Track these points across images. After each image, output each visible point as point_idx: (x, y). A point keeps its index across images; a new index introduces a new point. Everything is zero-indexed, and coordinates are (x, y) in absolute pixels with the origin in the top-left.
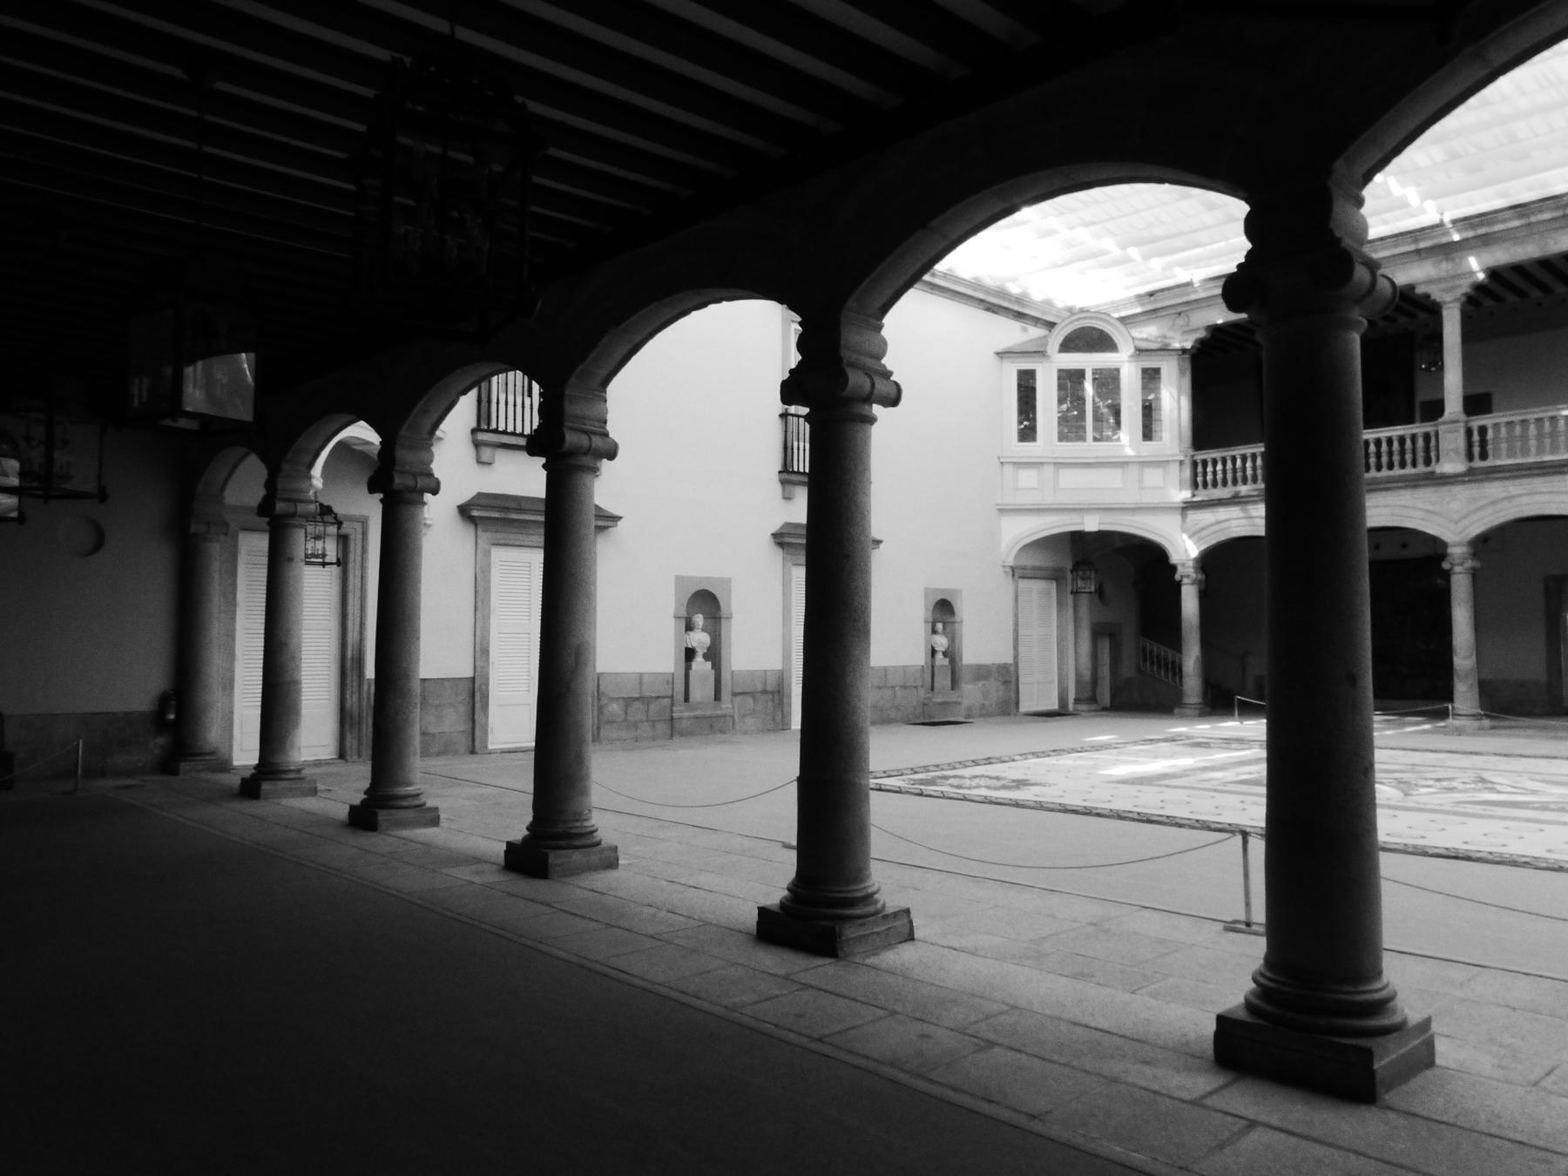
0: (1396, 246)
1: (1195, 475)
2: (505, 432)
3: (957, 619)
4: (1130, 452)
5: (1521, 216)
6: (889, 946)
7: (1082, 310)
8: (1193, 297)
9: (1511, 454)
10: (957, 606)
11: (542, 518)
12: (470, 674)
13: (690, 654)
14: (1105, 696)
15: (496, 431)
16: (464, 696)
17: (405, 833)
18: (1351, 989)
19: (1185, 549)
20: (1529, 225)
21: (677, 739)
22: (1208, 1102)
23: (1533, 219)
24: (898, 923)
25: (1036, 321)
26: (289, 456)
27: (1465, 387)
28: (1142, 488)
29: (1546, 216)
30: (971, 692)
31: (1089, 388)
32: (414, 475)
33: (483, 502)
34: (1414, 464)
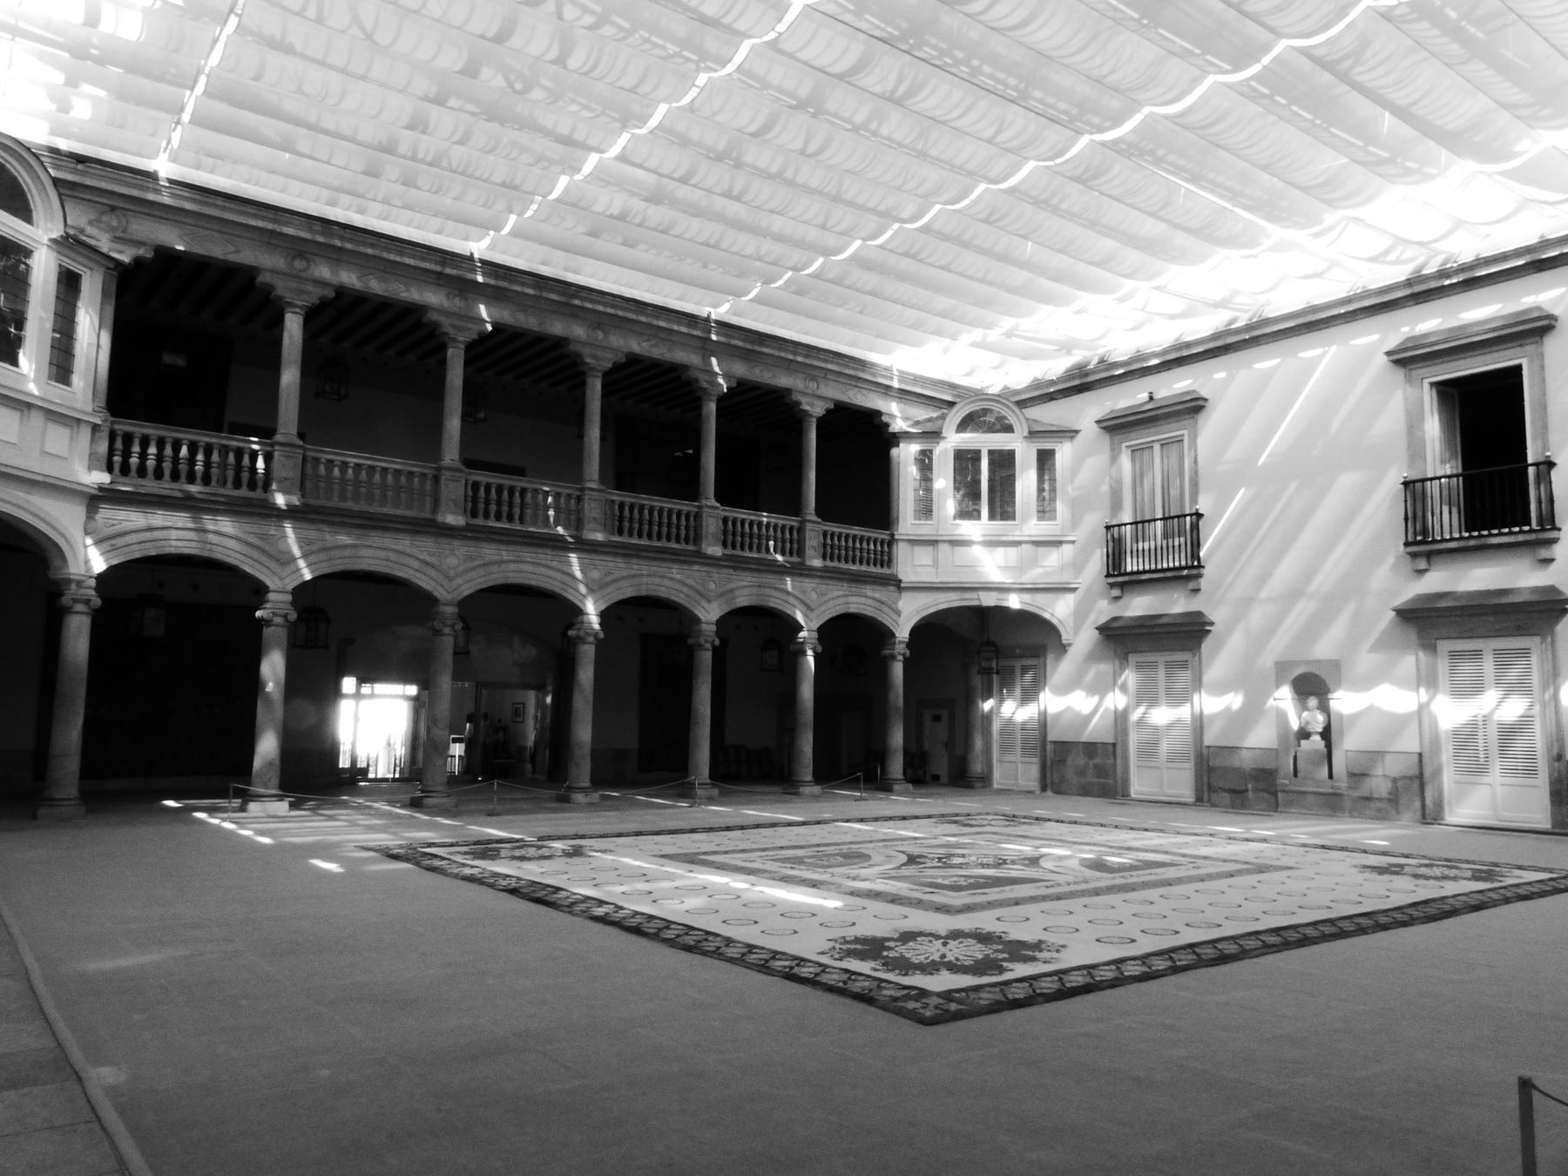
0: (424, 259)
5: (535, 287)
8: (151, 197)
9: (396, 504)
20: (540, 298)
23: (545, 294)
29: (554, 297)
34: (742, 548)
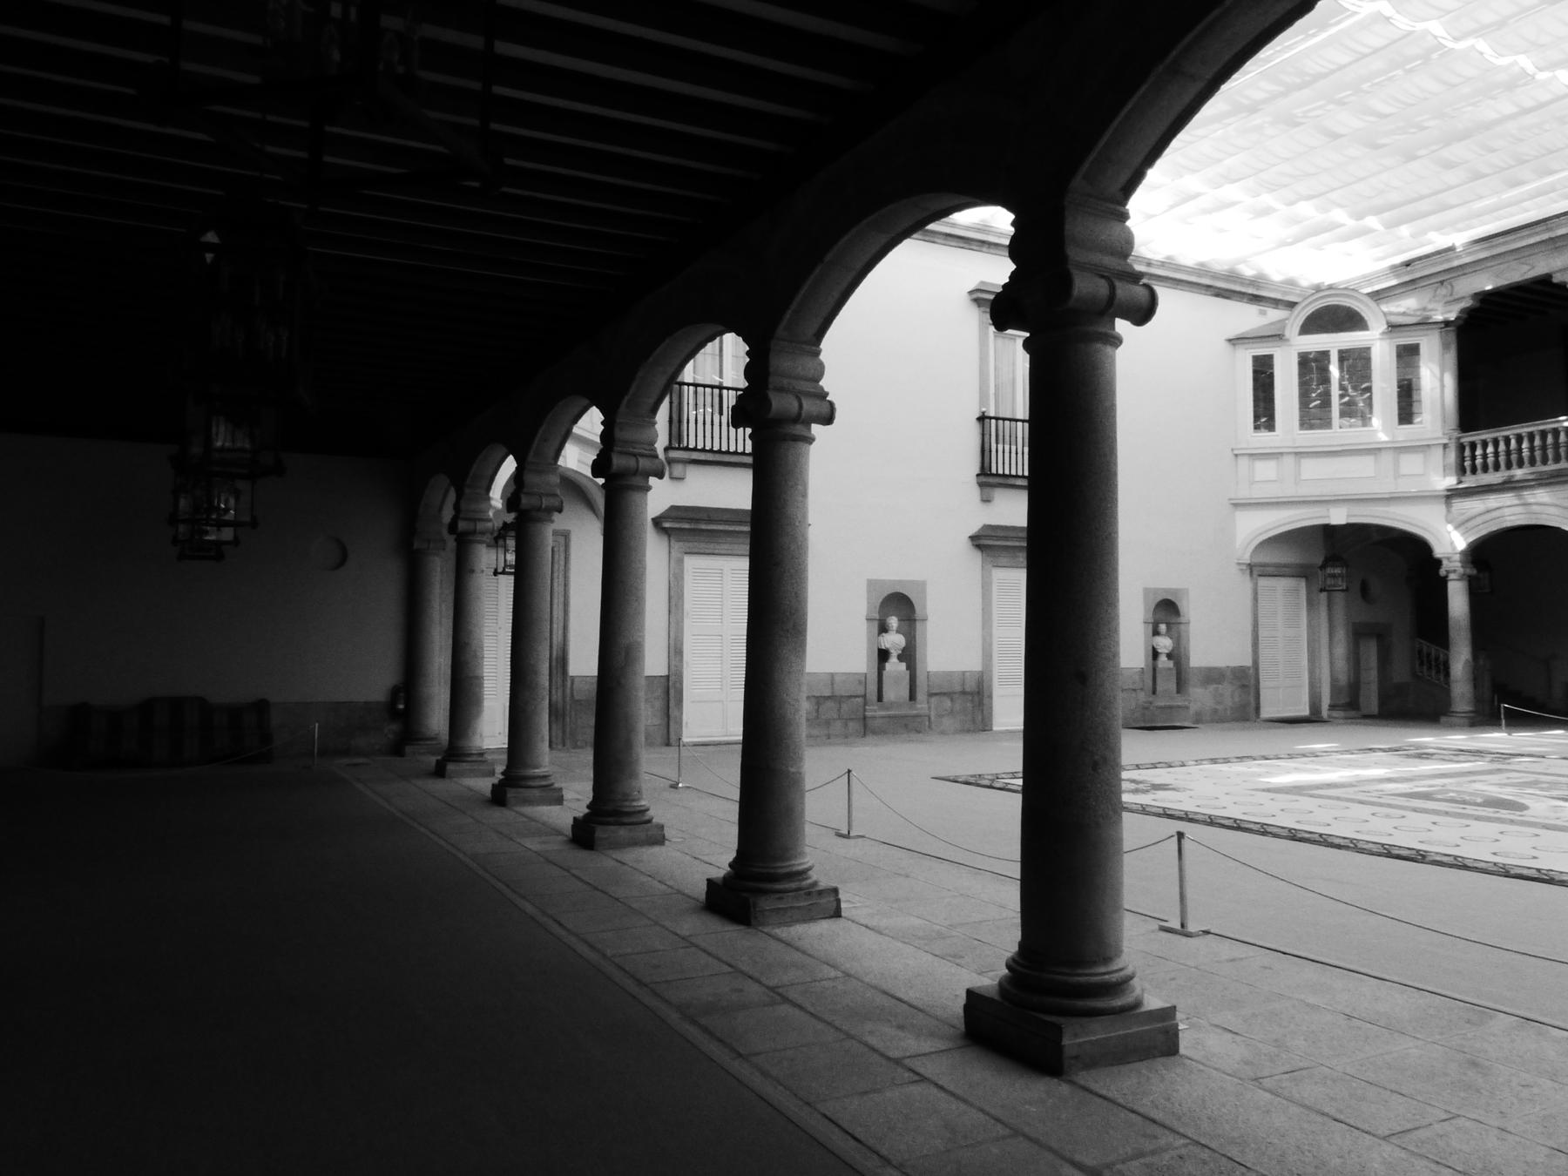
1: (1462, 459)
2: (695, 449)
3: (1182, 619)
4: (1383, 437)
6: (811, 919)
7: (1330, 287)
8: (1456, 263)
10: (1183, 606)
11: (747, 528)
12: (664, 672)
13: (883, 655)
14: (1371, 701)
15: (687, 449)
16: (659, 692)
17: (528, 810)
18: (1103, 970)
19: (1451, 540)
21: (870, 738)
22: (907, 1062)
24: (823, 901)
25: (1276, 303)
26: (468, 481)
27: (1399, 373)
28: (1397, 475)
30: (1200, 697)
31: (1334, 371)
32: (541, 496)
33: (674, 514)
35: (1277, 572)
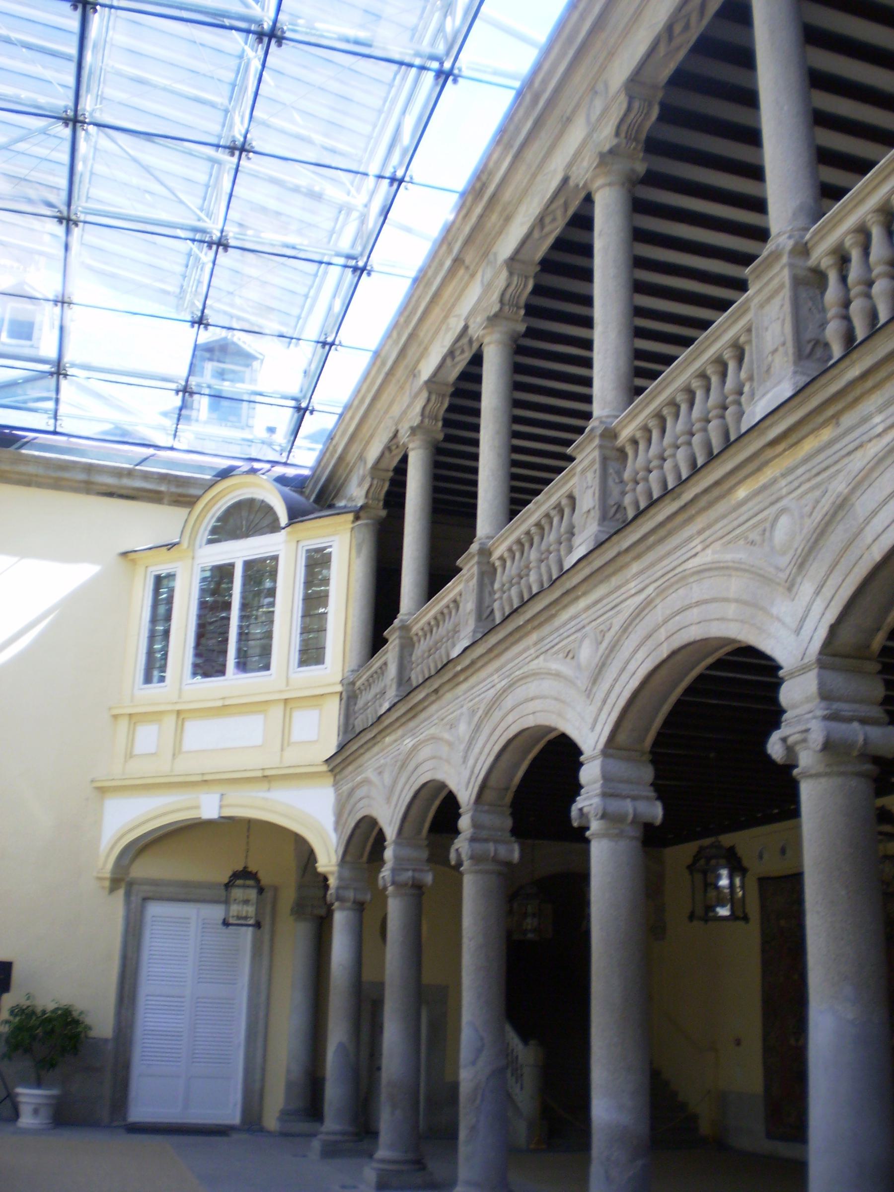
34: (256, 657)
35: (186, 893)
